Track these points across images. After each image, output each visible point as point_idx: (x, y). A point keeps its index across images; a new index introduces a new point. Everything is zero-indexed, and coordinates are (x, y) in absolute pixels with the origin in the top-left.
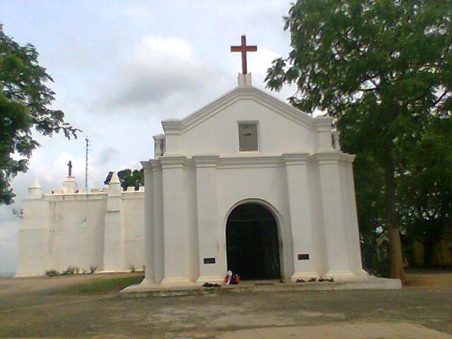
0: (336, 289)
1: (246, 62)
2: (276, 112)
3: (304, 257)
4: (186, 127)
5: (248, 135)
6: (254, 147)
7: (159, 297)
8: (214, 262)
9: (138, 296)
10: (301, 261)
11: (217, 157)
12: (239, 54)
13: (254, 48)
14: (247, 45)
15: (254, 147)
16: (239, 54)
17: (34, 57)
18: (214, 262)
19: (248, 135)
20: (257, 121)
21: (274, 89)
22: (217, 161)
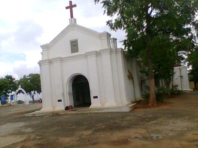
0: (100, 112)
1: (71, 13)
2: (88, 34)
3: (60, 101)
4: (51, 46)
5: (74, 46)
6: (77, 51)
7: (24, 117)
8: (97, 98)
9: (29, 116)
10: (94, 99)
11: (61, 58)
12: (69, 10)
13: (75, 6)
14: (73, 4)
15: (77, 51)
16: (69, 10)
17: (125, 41)
18: (97, 98)
19: (74, 46)
20: (77, 39)
21: (112, 30)
22: (61, 60)
